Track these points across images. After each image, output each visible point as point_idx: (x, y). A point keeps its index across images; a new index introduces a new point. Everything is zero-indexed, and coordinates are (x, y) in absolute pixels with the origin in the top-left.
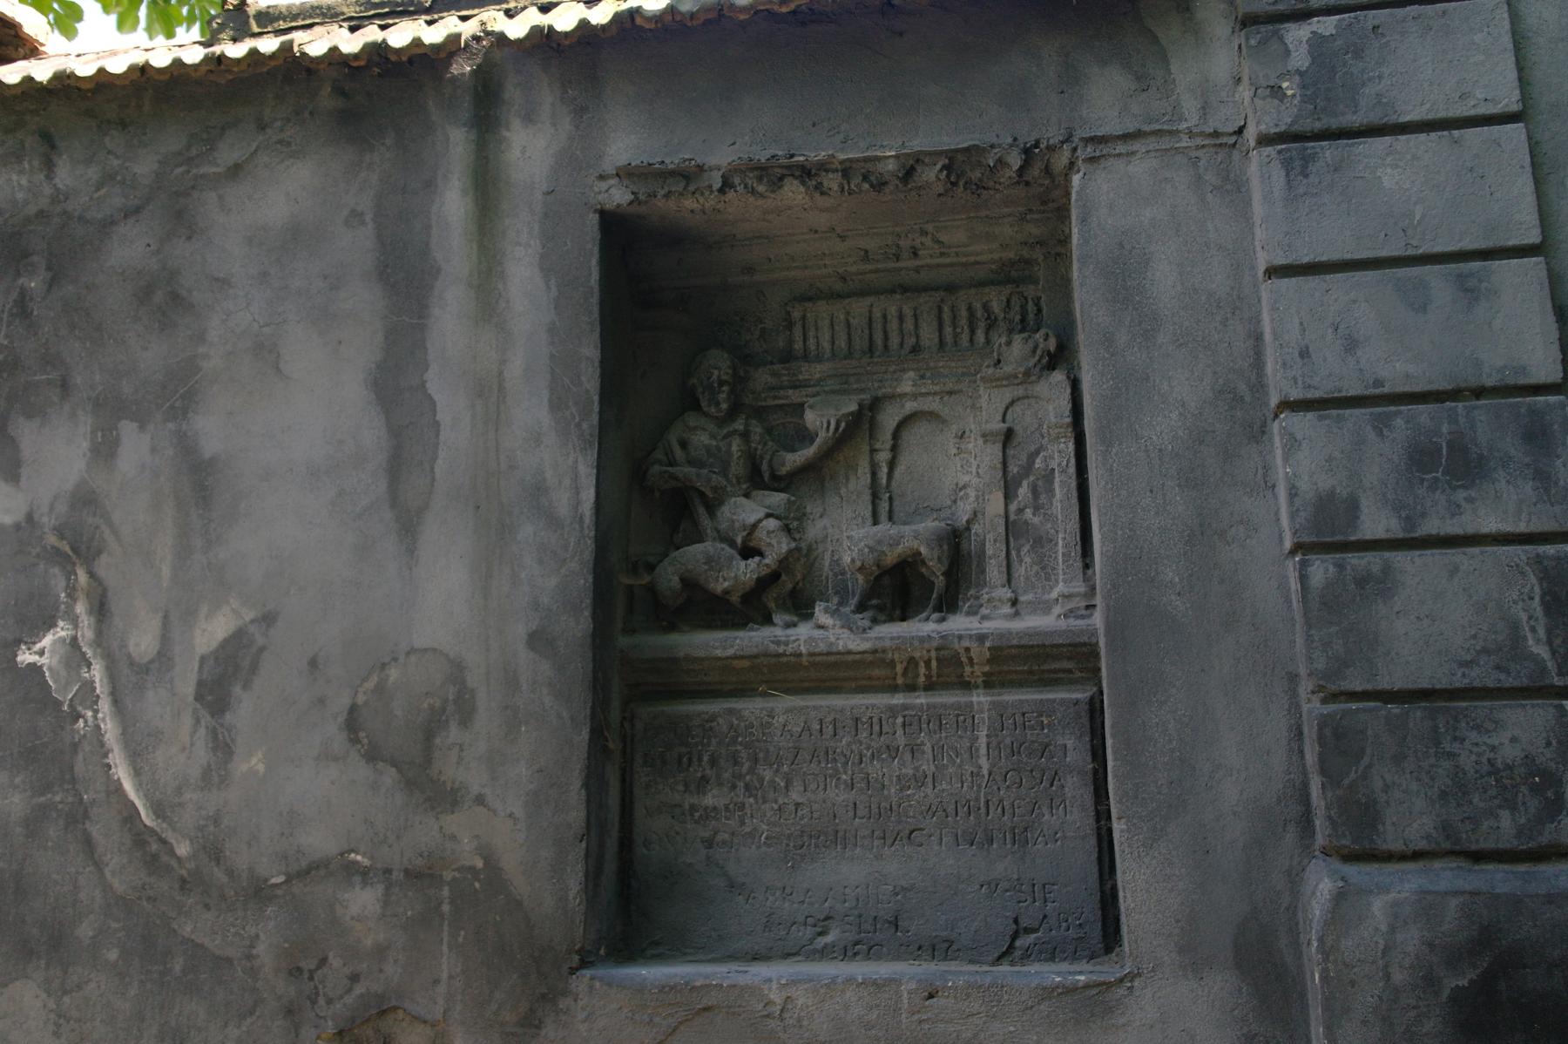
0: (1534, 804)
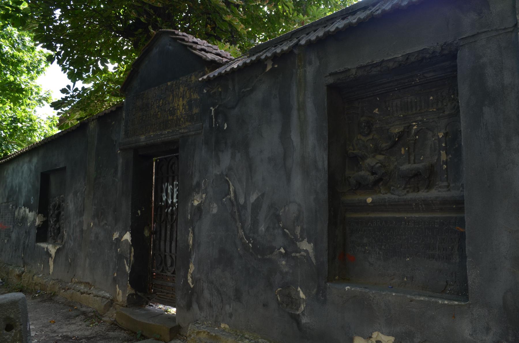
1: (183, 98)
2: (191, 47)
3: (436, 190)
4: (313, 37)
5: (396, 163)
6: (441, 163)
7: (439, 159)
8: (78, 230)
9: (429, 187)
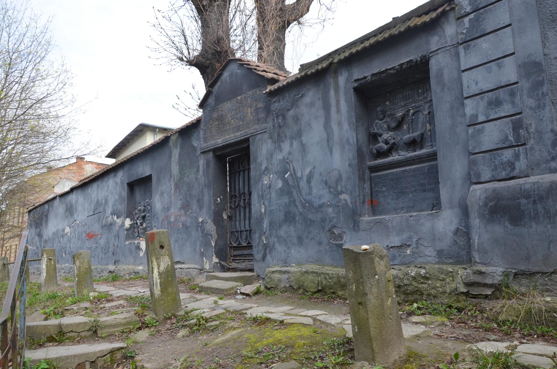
0: (509, 169)
1: (251, 108)
2: (255, 69)
4: (342, 57)
8: (166, 222)
9: (421, 148)
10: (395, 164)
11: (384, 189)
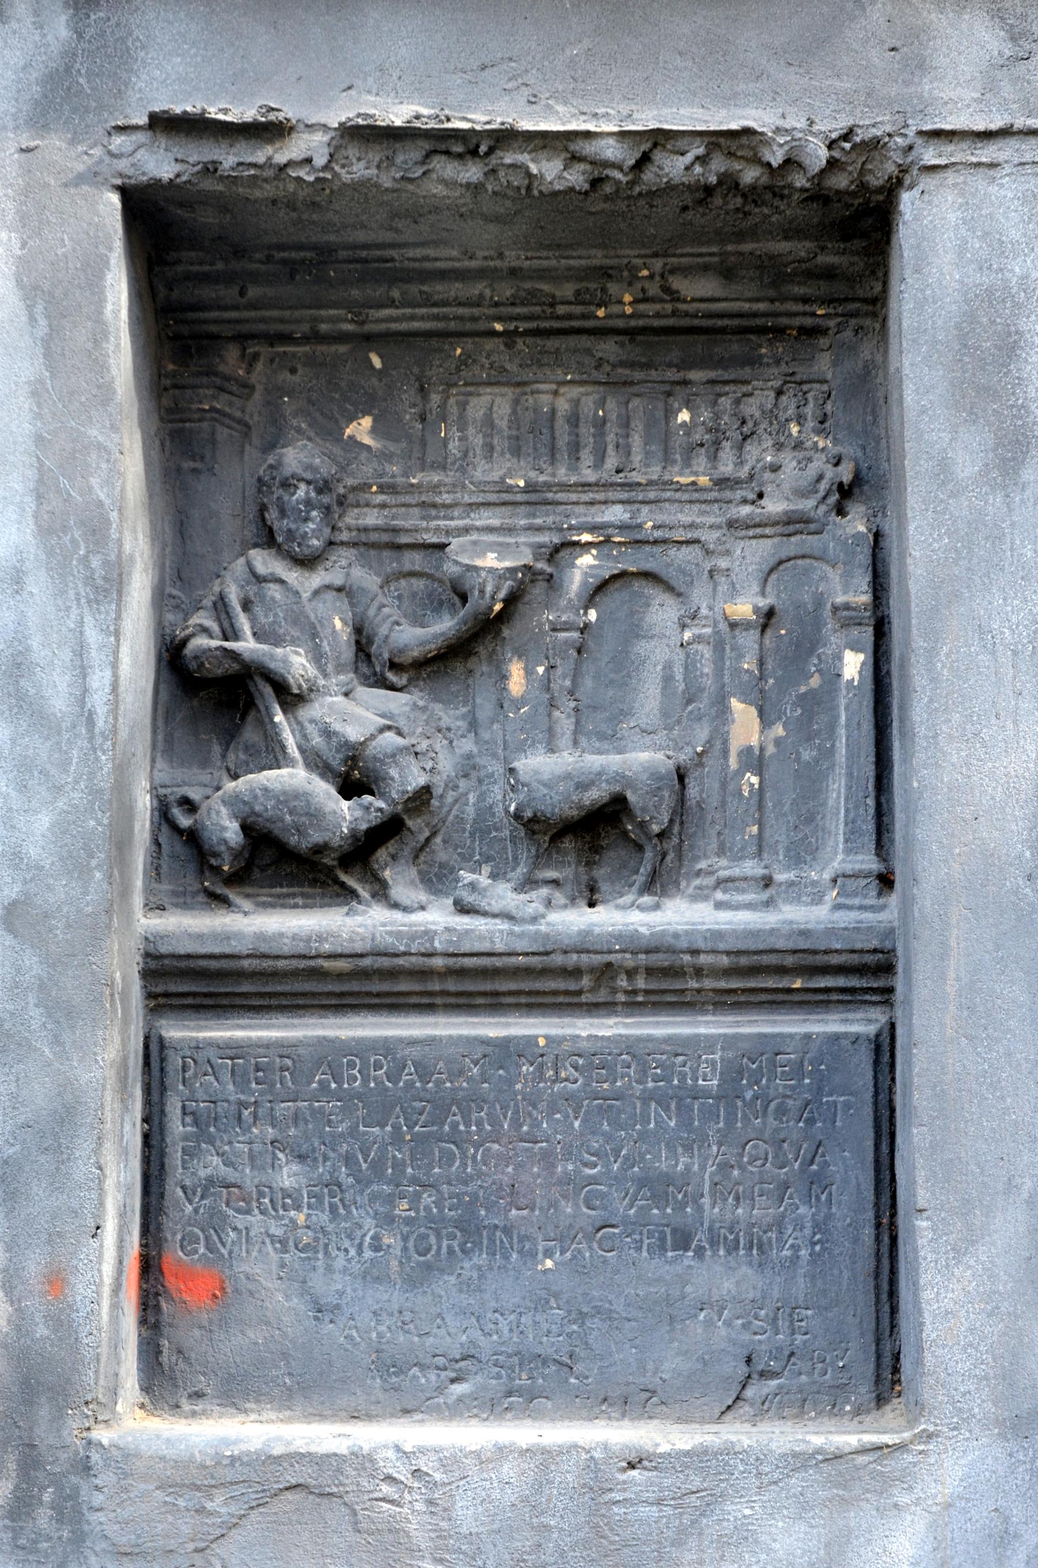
3: (694, 898)
5: (467, 745)
6: (733, 762)
7: (719, 740)
9: (657, 884)
10: (423, 974)
11: (288, 1176)
